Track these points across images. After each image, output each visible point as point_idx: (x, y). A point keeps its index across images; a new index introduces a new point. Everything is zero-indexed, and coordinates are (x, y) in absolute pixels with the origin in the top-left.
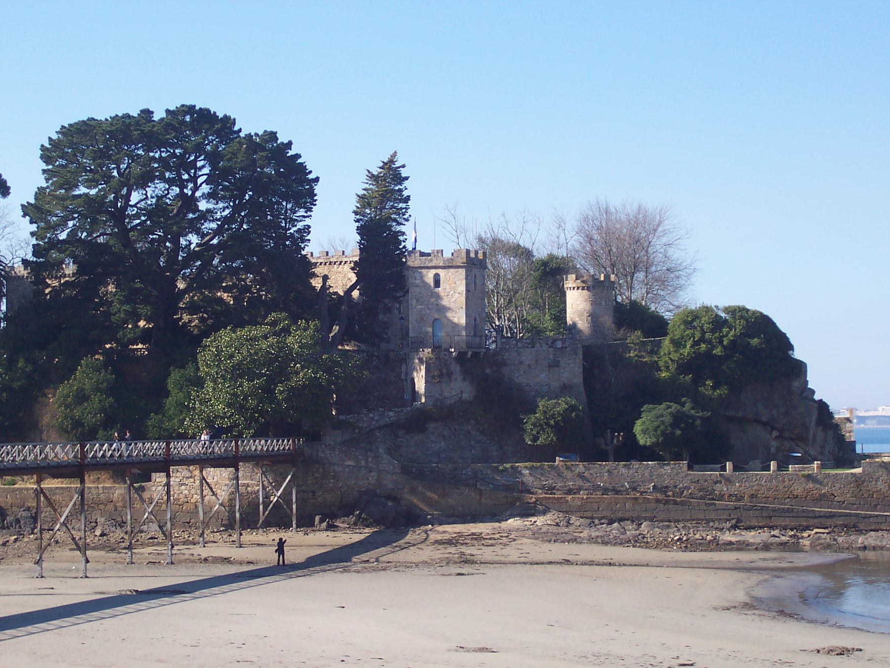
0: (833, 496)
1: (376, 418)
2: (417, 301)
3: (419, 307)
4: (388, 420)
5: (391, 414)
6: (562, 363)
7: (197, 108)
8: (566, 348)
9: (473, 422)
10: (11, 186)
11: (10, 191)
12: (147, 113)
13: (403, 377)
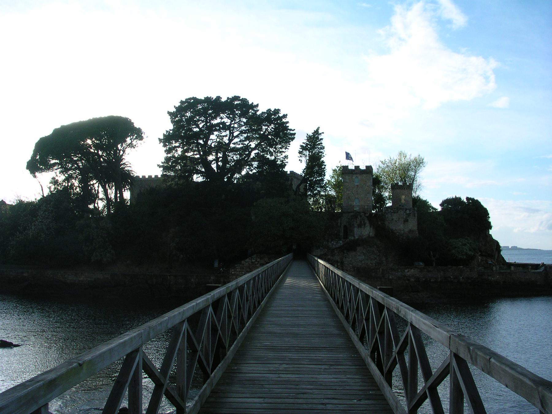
0: (63, 343)
1: (335, 244)
2: (347, 189)
3: (348, 192)
4: (340, 245)
5: (341, 242)
6: (409, 220)
7: (241, 98)
8: (411, 213)
9: (375, 247)
10: (134, 122)
11: (141, 128)
12: (219, 98)
13: (339, 225)
